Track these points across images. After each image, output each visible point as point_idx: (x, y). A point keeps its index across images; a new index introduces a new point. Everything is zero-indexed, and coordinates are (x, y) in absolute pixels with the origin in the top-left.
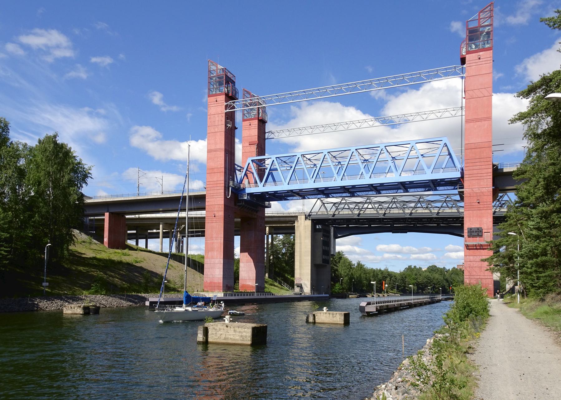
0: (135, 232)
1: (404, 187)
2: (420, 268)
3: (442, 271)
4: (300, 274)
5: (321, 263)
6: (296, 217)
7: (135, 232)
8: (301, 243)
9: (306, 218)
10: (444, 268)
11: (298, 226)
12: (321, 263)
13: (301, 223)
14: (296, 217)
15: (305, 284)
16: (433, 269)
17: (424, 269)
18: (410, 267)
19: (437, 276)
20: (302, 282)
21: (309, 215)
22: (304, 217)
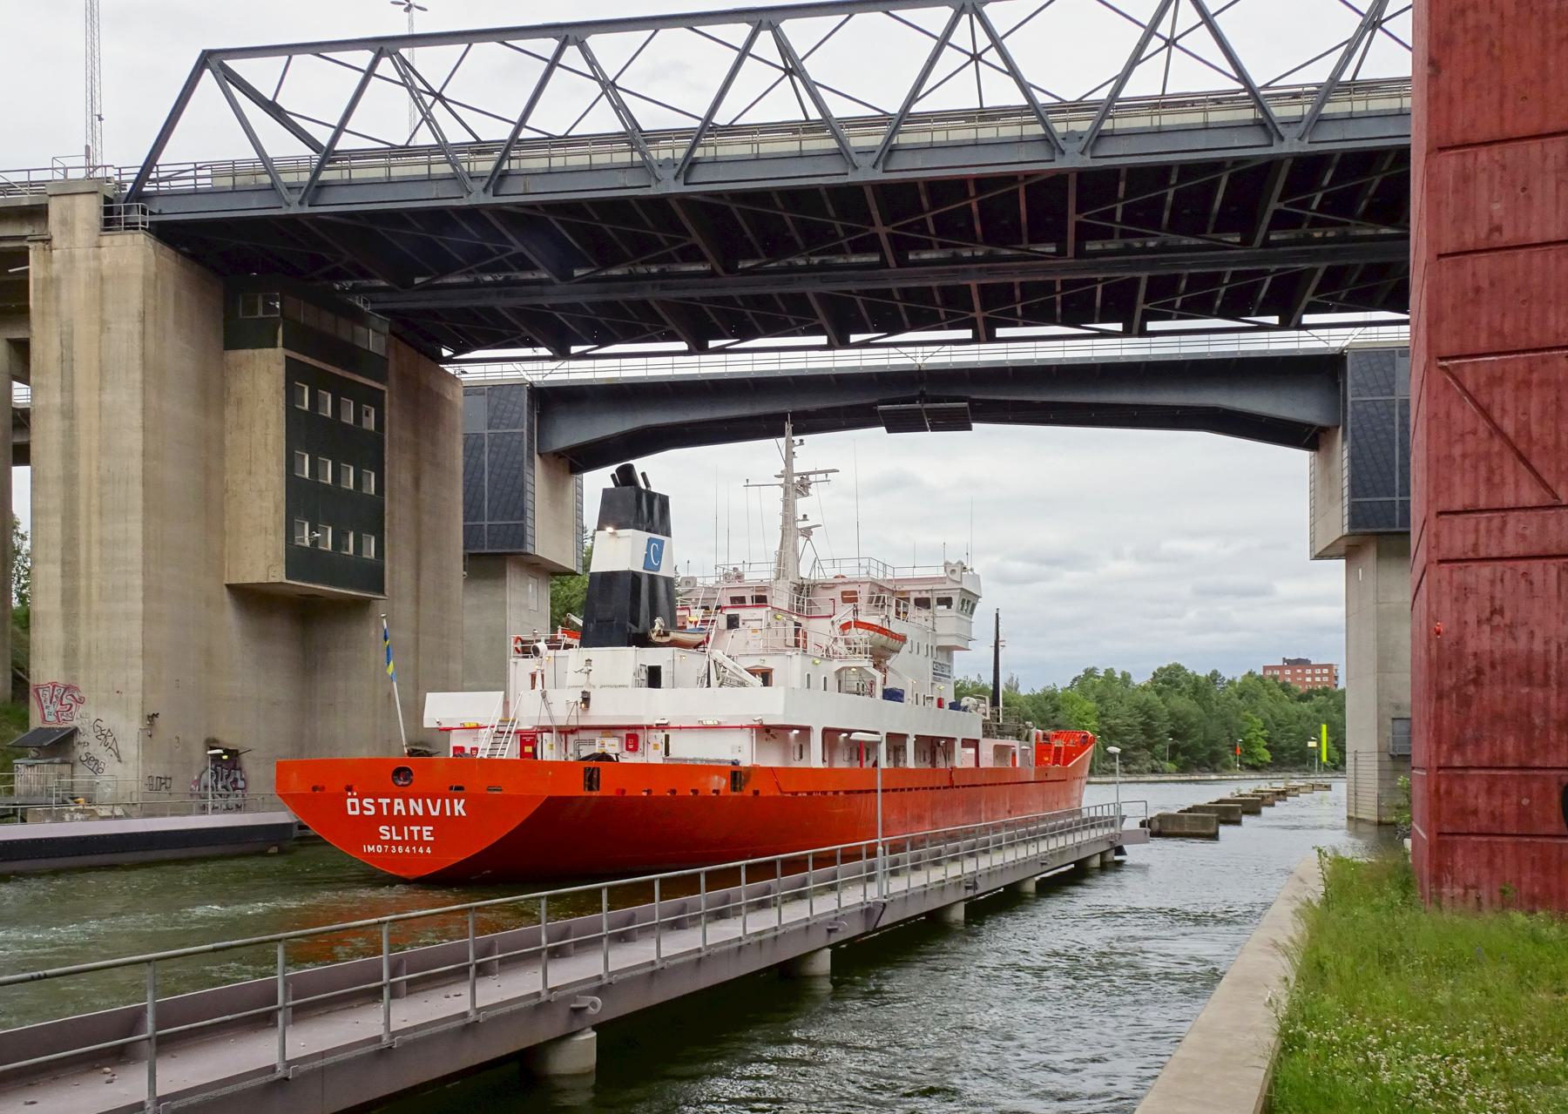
0: (1324, 727)
1: (1038, 113)
2: (1126, 678)
3: (1201, 689)
4: (70, 655)
5: (278, 575)
6: (37, 213)
7: (1324, 727)
8: (69, 413)
9: (111, 219)
10: (1215, 673)
11: (51, 283)
12: (278, 575)
13: (71, 259)
14: (37, 213)
15: (105, 736)
16: (1170, 679)
17: (1141, 678)
18: (1090, 673)
19: (1182, 704)
20: (82, 718)
21: (137, 195)
22: (87, 210)
